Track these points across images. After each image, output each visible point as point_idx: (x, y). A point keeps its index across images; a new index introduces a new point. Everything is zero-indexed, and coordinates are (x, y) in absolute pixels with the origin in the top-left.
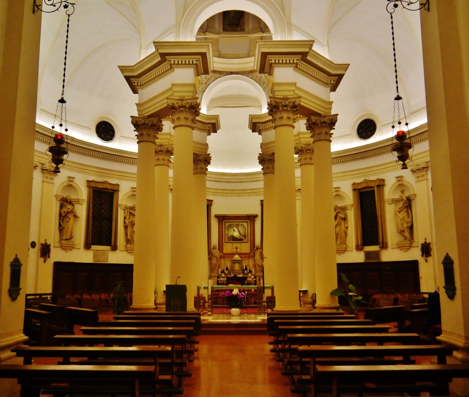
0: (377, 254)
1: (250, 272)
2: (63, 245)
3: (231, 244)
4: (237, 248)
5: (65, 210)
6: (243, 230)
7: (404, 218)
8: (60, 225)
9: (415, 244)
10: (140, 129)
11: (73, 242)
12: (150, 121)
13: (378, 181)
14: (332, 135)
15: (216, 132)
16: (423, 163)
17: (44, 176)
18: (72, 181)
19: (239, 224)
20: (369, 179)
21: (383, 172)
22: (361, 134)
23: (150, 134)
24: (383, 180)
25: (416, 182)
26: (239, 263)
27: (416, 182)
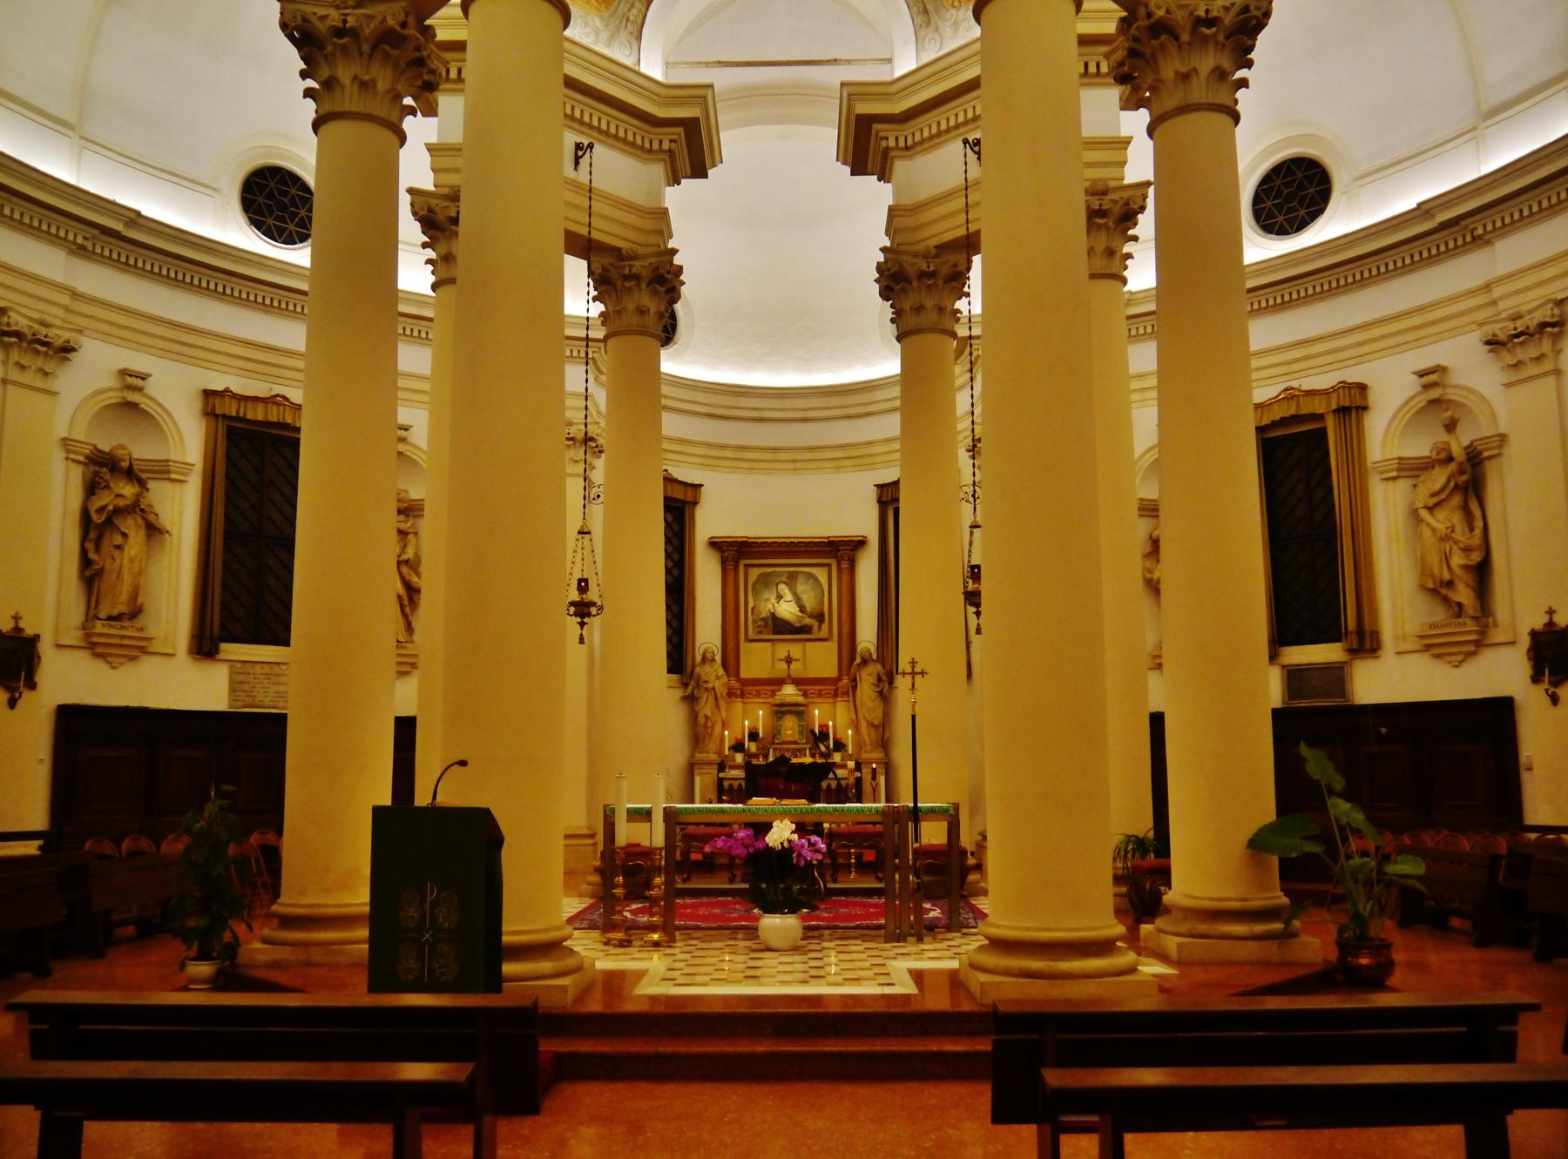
0: (1335, 676)
1: (840, 746)
2: (95, 640)
3: (770, 644)
4: (789, 660)
5: (104, 499)
6: (813, 594)
7: (1452, 531)
8: (85, 562)
9: (1498, 636)
10: (326, 57)
11: (142, 629)
12: (370, 17)
13: (1341, 391)
14: (1129, 262)
15: (706, 176)
16: (1544, 304)
17: (11, 361)
18: (140, 389)
19: (797, 572)
20: (1300, 386)
21: (1360, 359)
22: (1270, 216)
23: (374, 82)
24: (1362, 388)
25: (1508, 385)
26: (799, 714)
27: (1508, 385)
